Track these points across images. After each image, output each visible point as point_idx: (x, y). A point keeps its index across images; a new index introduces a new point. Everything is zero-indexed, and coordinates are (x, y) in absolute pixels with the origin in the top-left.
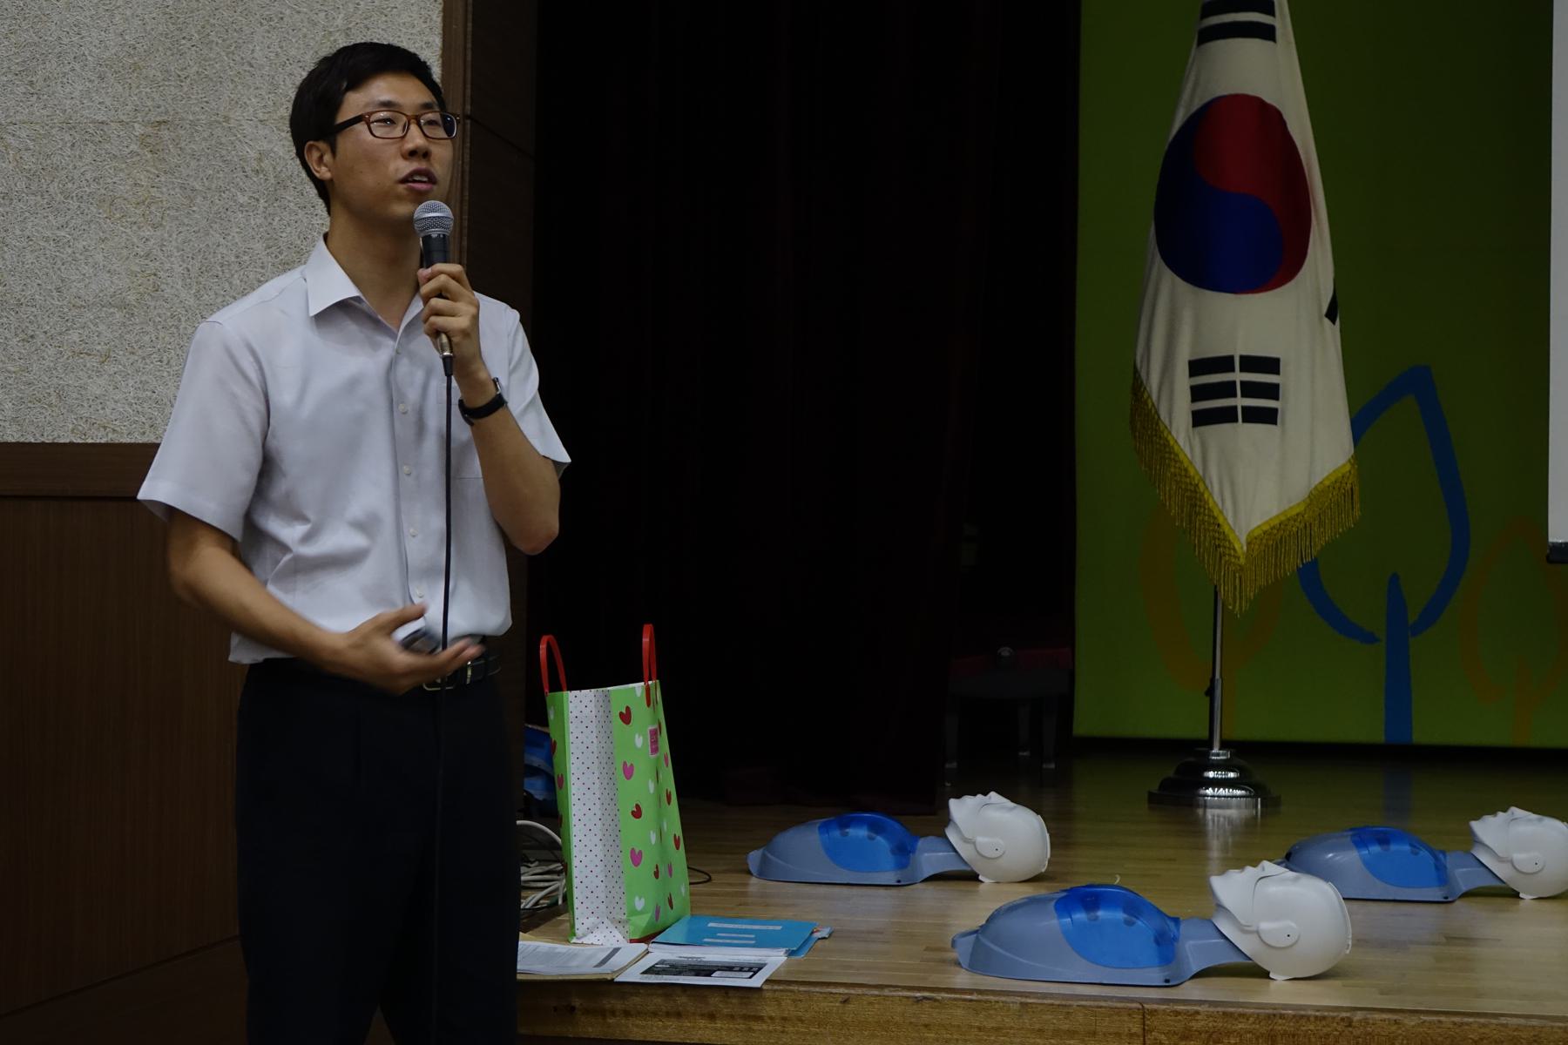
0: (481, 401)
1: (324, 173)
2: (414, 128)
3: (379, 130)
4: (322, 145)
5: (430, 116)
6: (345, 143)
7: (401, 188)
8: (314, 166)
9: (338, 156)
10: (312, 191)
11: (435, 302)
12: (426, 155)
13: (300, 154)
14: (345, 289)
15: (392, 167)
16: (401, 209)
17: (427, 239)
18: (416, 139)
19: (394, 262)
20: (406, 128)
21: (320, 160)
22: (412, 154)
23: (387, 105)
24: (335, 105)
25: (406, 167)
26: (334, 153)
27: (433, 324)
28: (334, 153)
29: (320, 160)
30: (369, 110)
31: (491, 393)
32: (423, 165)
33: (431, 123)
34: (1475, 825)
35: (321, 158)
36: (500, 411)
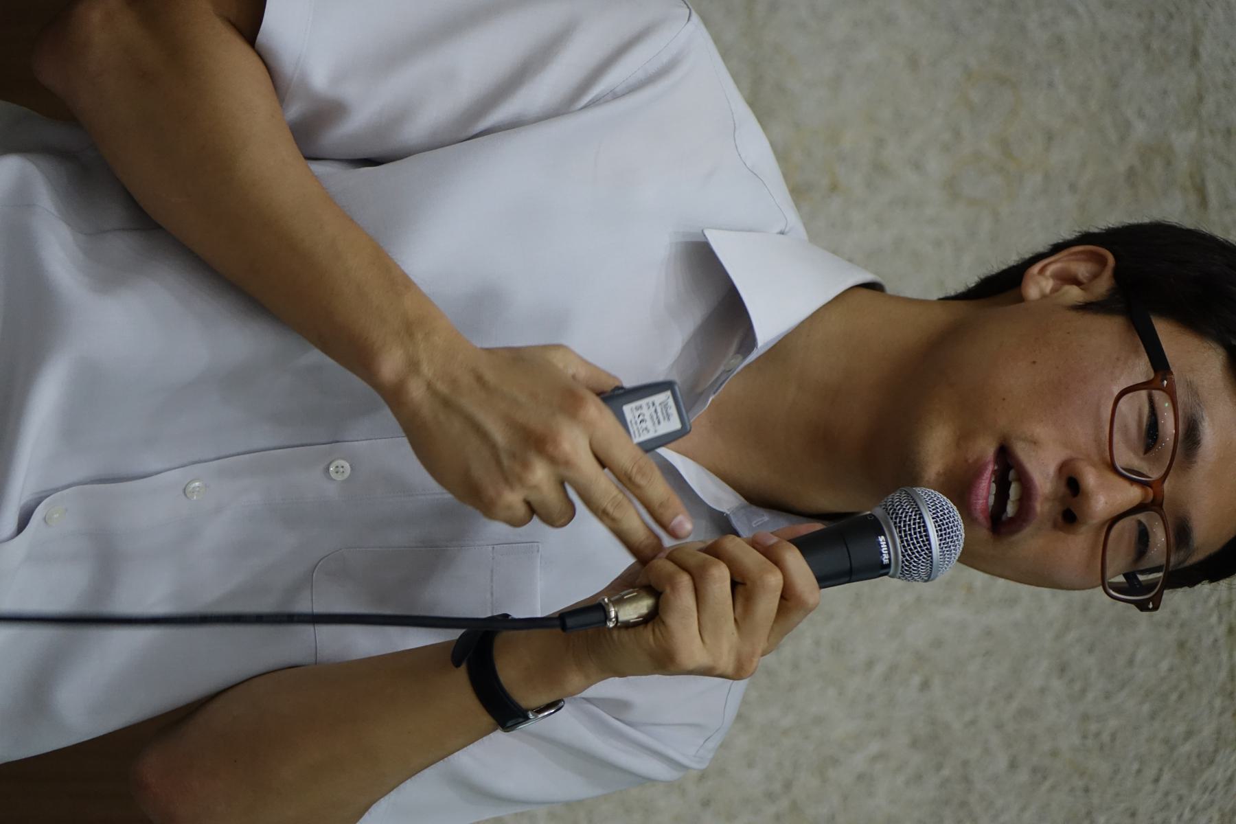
0: (510, 672)
1: (1038, 286)
2: (1134, 494)
3: (1132, 410)
4: (1103, 285)
5: (1159, 537)
6: (1106, 336)
7: (986, 449)
8: (1056, 265)
9: (1073, 315)
10: (996, 263)
11: (720, 577)
12: (1069, 517)
13: (1086, 238)
14: (771, 319)
15: (1041, 431)
16: (937, 447)
17: (875, 528)
18: (1107, 497)
19: (823, 442)
20: (1131, 477)
21: (1068, 279)
22: (1072, 485)
23: (1190, 436)
24: (1195, 319)
25: (1042, 470)
26: (1086, 308)
27: (672, 581)
28: (1086, 308)
29: (1068, 279)
30: (1180, 392)
31: (525, 698)
32: (1041, 507)
33: (1143, 537)
34: (463, 668)
35: (1075, 281)
36: (486, 719)
